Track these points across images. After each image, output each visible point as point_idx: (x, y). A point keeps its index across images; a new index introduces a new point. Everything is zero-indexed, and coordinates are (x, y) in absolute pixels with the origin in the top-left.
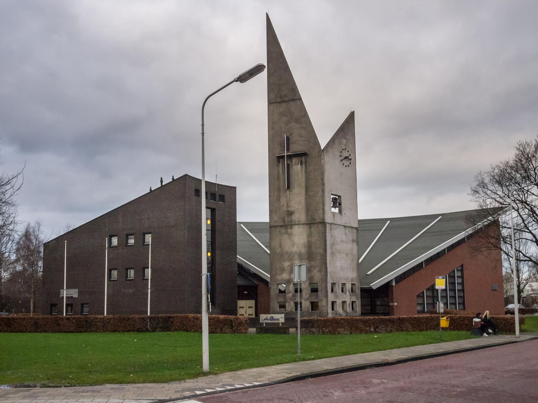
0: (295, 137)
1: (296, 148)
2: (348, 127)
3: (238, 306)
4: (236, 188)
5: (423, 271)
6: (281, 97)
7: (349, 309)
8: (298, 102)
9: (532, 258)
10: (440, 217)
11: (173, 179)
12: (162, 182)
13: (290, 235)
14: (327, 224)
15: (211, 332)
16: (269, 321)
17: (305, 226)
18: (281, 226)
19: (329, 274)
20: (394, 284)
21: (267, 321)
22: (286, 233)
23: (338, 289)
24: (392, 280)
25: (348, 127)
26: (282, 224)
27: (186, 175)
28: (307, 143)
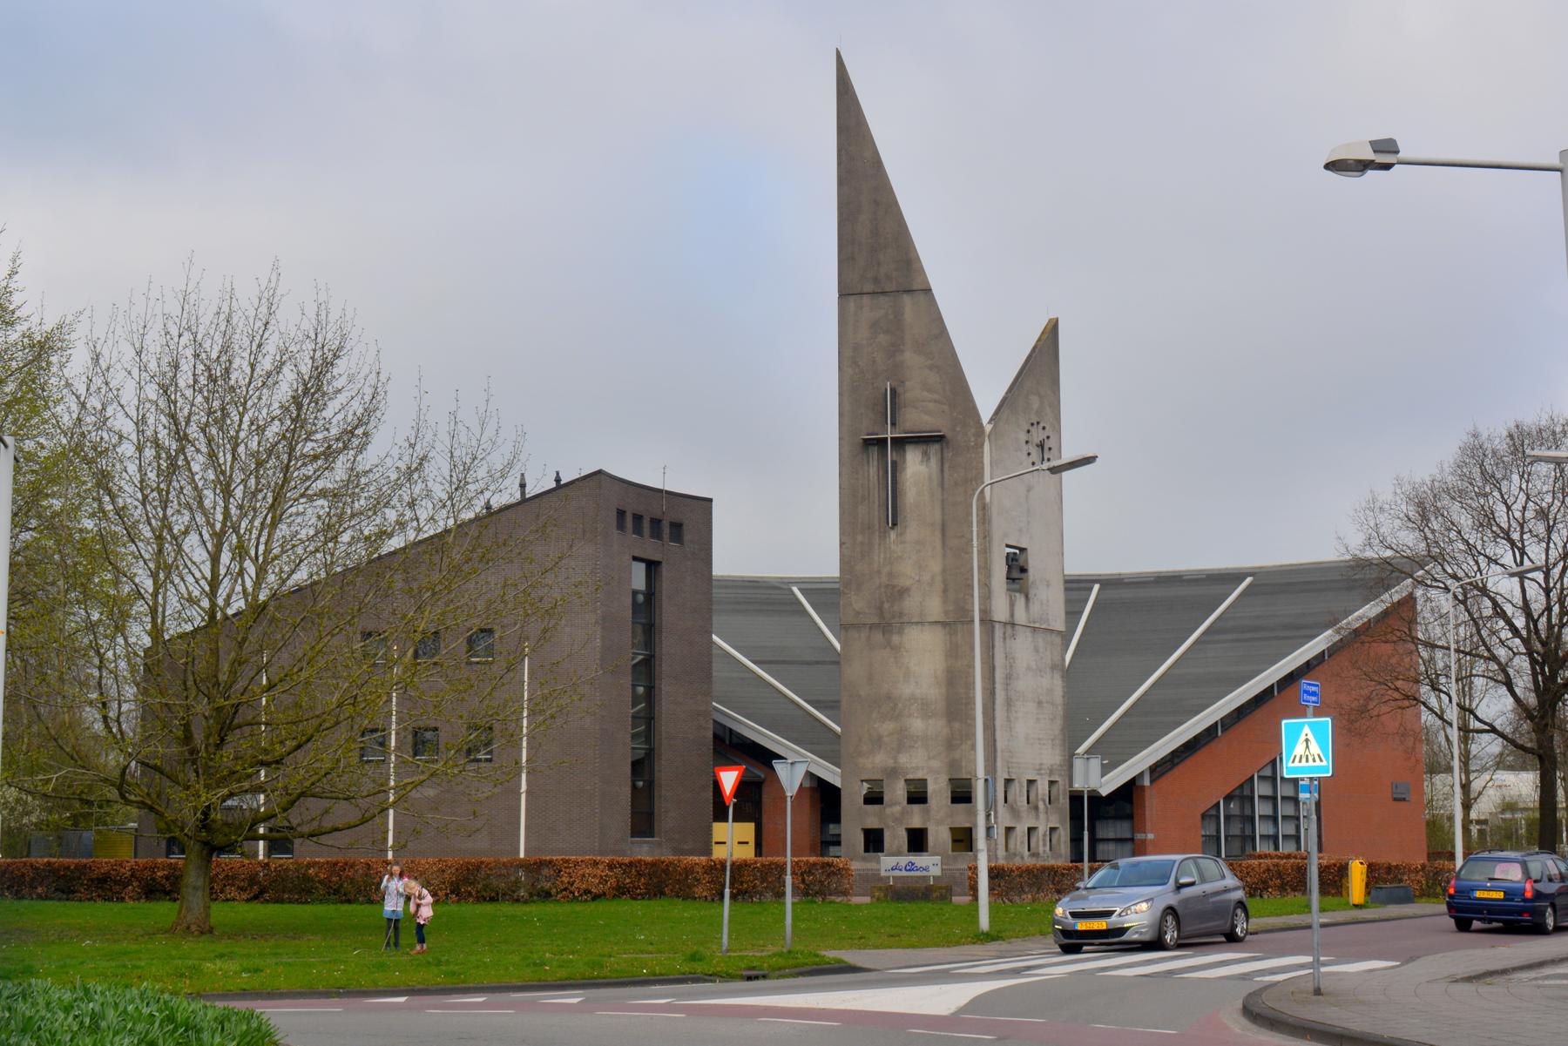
0: (913, 391)
1: (917, 419)
2: (1042, 363)
3: (715, 839)
4: (710, 500)
5: (1219, 747)
6: (876, 280)
7: (1042, 848)
8: (922, 297)
9: (1497, 725)
10: (1249, 580)
11: (558, 480)
12: (523, 486)
13: (896, 649)
14: (997, 626)
15: (1144, 854)
16: (904, 873)
17: (939, 628)
18: (872, 627)
19: (999, 754)
20: (1147, 782)
21: (897, 873)
22: (888, 644)
23: (1018, 793)
24: (1142, 774)
25: (1042, 363)
26: (876, 620)
27: (600, 472)
28: (946, 408)
